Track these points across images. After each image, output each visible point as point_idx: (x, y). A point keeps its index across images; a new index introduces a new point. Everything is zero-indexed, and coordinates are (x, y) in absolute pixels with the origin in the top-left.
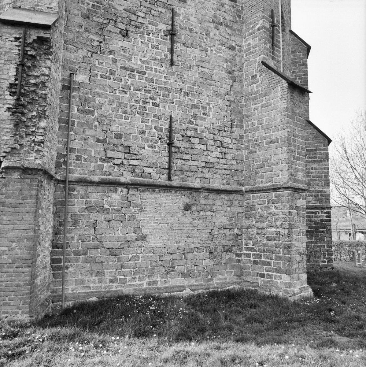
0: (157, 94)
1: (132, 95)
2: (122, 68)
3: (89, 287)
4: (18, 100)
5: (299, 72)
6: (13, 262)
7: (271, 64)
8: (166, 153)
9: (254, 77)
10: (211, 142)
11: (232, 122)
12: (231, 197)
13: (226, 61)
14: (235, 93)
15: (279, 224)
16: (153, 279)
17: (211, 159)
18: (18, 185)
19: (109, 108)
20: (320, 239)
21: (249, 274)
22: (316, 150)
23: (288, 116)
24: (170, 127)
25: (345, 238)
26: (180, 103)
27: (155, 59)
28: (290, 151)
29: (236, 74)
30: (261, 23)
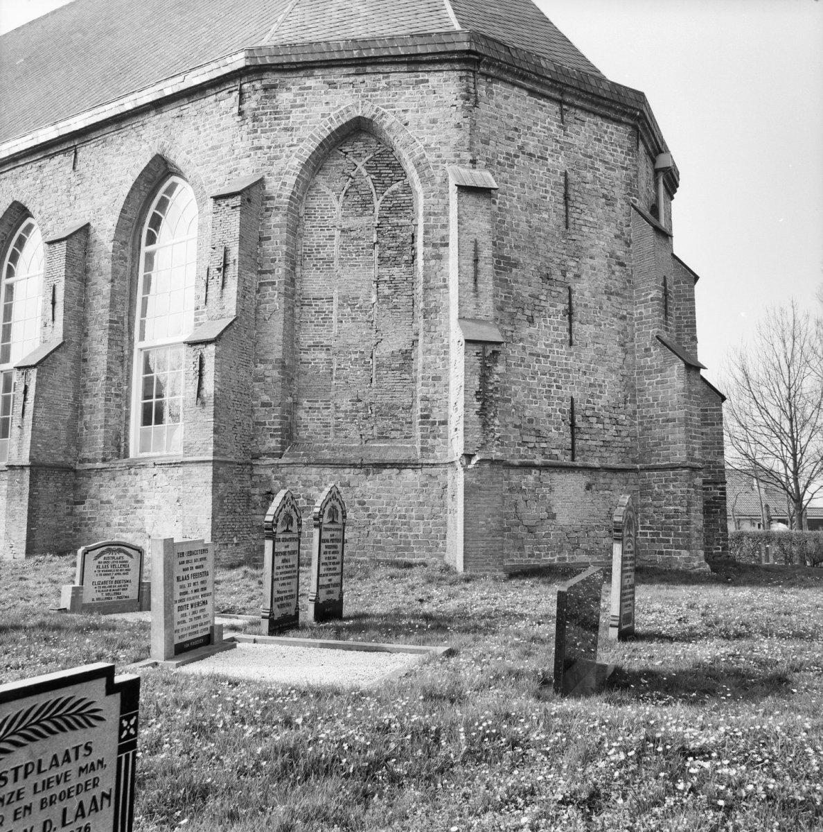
0: (560, 376)
1: (540, 380)
2: (530, 354)
3: (513, 561)
4: (483, 404)
5: (684, 309)
6: (490, 533)
7: (665, 336)
8: (568, 434)
9: (647, 350)
10: (607, 421)
11: (626, 397)
12: (626, 475)
13: (619, 333)
14: (628, 366)
15: (677, 502)
16: (562, 555)
17: (607, 437)
18: (489, 474)
19: (522, 394)
20: (713, 521)
21: (646, 553)
22: (706, 410)
23: (685, 396)
24: (572, 408)
25: (747, 527)
26: (579, 383)
27: (557, 341)
28: (688, 431)
29: (629, 345)
30: (653, 294)
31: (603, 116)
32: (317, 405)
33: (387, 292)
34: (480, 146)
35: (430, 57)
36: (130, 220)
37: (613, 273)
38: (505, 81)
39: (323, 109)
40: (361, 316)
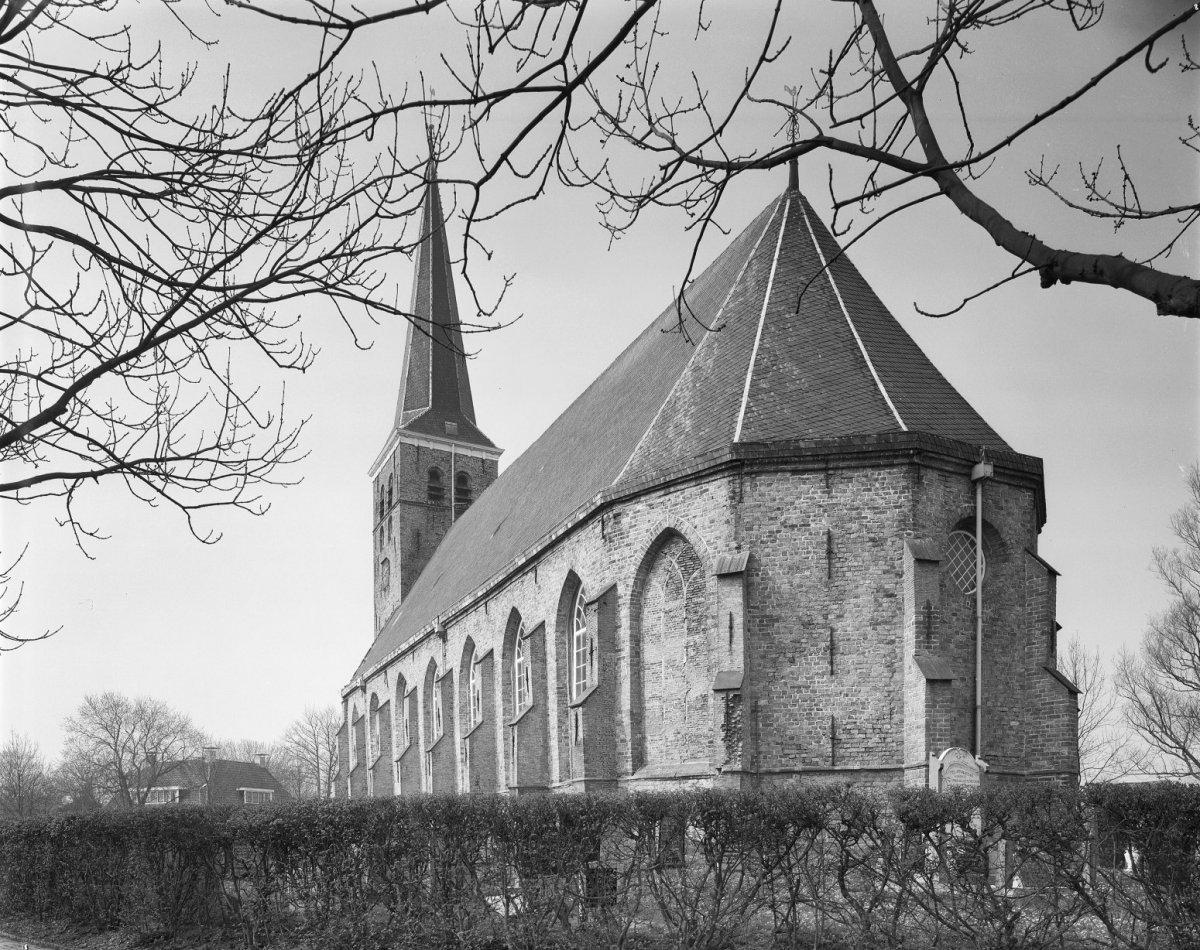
1: (800, 706)
31: (873, 467)
32: (655, 738)
33: (693, 653)
34: (744, 534)
35: (707, 472)
36: (565, 615)
37: (880, 605)
38: (768, 472)
39: (646, 526)
40: (679, 674)
